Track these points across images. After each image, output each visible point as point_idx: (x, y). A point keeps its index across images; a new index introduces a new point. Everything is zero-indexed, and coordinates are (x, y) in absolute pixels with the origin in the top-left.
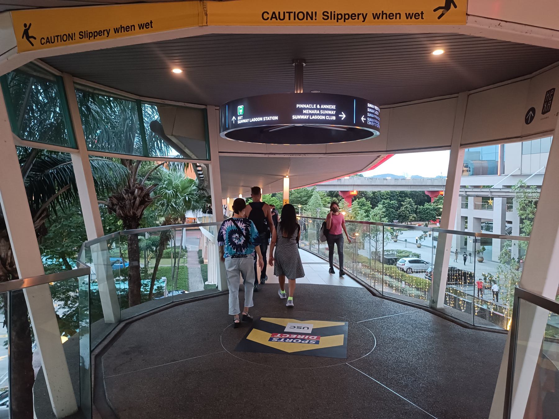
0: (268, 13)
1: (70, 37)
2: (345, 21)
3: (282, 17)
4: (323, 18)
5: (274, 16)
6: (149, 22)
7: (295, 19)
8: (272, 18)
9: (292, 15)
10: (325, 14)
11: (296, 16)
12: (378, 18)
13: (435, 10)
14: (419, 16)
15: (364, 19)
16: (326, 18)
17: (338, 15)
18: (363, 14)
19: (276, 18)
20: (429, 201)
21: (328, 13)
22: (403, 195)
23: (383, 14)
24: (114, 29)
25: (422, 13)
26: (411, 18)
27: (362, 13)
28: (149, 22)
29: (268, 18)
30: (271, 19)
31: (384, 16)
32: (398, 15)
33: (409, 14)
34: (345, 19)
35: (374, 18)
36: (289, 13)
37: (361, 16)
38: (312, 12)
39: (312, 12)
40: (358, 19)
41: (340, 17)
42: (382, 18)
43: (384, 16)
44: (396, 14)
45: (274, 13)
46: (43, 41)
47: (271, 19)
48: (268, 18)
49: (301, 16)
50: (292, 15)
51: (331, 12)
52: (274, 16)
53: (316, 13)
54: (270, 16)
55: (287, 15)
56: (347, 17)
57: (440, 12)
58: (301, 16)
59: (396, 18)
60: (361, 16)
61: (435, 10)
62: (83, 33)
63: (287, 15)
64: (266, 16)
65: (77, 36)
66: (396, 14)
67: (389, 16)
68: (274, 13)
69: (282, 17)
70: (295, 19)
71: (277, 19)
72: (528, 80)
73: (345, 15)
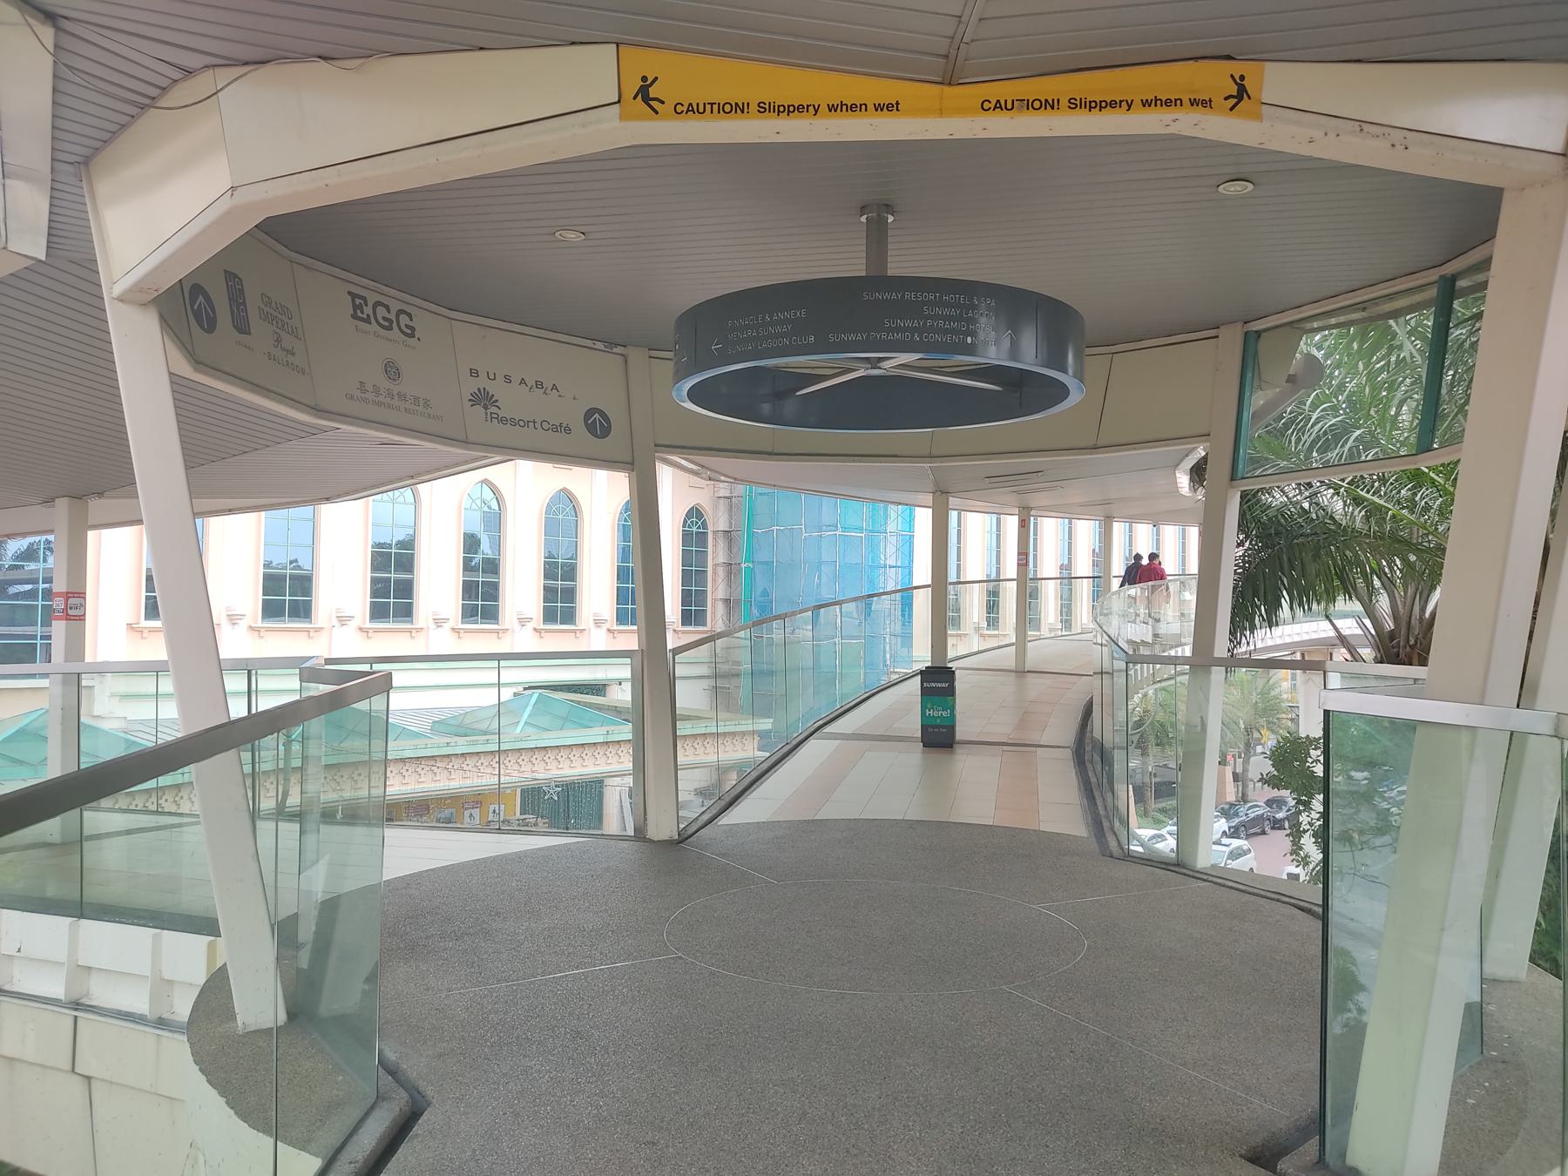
0: (682, 105)
1: (739, 109)
2: (788, 115)
3: (701, 110)
4: (1069, 107)
5: (690, 109)
6: (894, 103)
7: (719, 112)
8: (688, 111)
9: (715, 107)
10: (1072, 101)
11: (721, 109)
12: (835, 111)
13: (1226, 99)
14: (893, 106)
15: (816, 111)
16: (1073, 106)
17: (1090, 102)
18: (1127, 101)
19: (693, 110)
20: (285, 780)
21: (765, 104)
22: (186, 466)
23: (1156, 100)
24: (875, 104)
25: (897, 103)
26: (882, 110)
27: (812, 103)
28: (894, 103)
29: (682, 111)
30: (687, 113)
31: (844, 107)
32: (863, 107)
33: (879, 105)
34: (789, 111)
35: (830, 111)
36: (712, 104)
37: (811, 108)
38: (1053, 100)
39: (1053, 100)
40: (808, 111)
41: (1093, 104)
42: (841, 111)
43: (844, 107)
44: (861, 105)
45: (691, 104)
46: (679, 108)
47: (687, 113)
48: (682, 111)
49: (1037, 105)
50: (715, 107)
51: (770, 103)
52: (690, 109)
53: (1058, 100)
54: (685, 109)
55: (708, 107)
56: (1104, 105)
57: (1232, 101)
58: (727, 108)
59: (1176, 105)
60: (811, 108)
61: (1226, 99)
62: (765, 104)
63: (708, 107)
64: (986, 105)
65: (753, 107)
66: (861, 105)
67: (851, 108)
68: (691, 104)
69: (701, 110)
70: (719, 112)
71: (1002, 110)
72: (212, 98)
73: (789, 106)
